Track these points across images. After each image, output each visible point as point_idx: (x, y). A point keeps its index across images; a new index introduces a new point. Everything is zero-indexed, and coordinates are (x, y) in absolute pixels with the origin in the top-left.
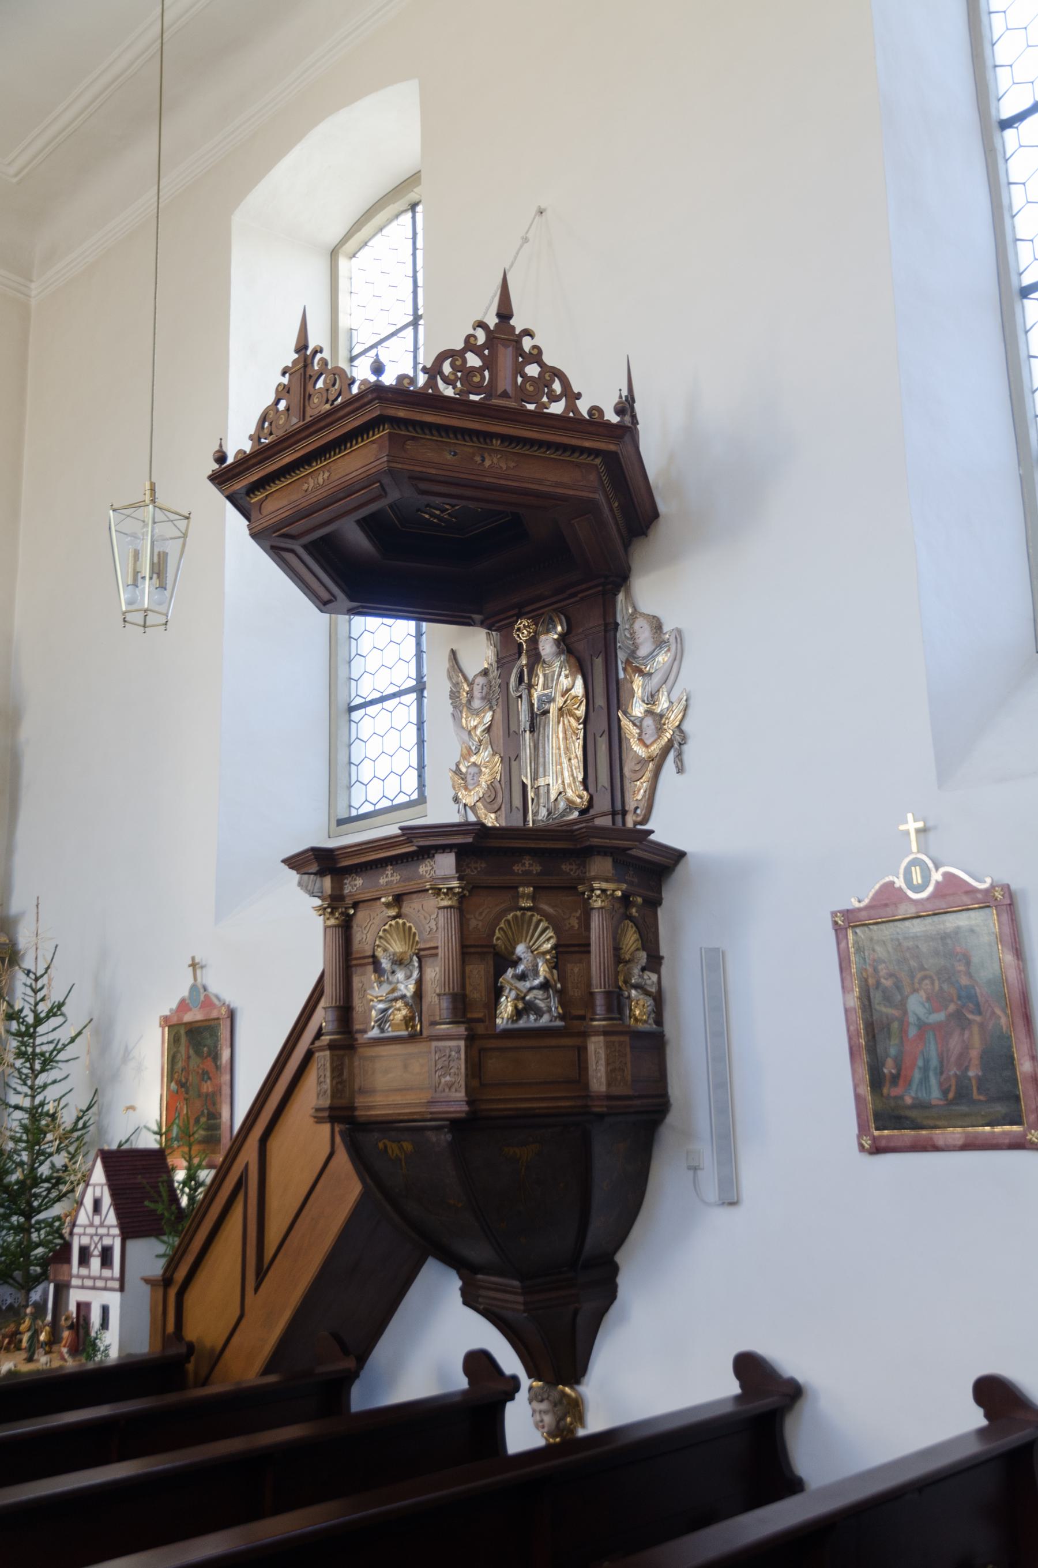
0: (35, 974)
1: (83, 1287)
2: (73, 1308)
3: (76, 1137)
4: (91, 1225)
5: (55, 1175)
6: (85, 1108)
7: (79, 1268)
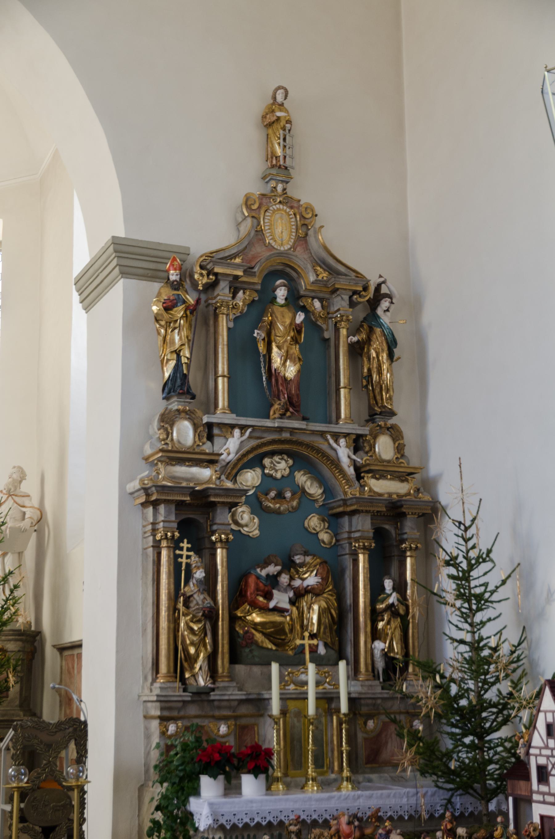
0: (464, 525)
1: (544, 802)
2: (537, 820)
3: (512, 669)
4: (547, 747)
5: (502, 701)
6: (516, 644)
7: (538, 785)
